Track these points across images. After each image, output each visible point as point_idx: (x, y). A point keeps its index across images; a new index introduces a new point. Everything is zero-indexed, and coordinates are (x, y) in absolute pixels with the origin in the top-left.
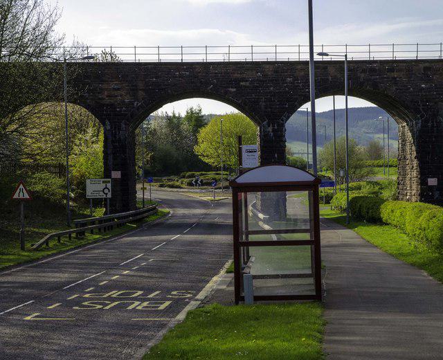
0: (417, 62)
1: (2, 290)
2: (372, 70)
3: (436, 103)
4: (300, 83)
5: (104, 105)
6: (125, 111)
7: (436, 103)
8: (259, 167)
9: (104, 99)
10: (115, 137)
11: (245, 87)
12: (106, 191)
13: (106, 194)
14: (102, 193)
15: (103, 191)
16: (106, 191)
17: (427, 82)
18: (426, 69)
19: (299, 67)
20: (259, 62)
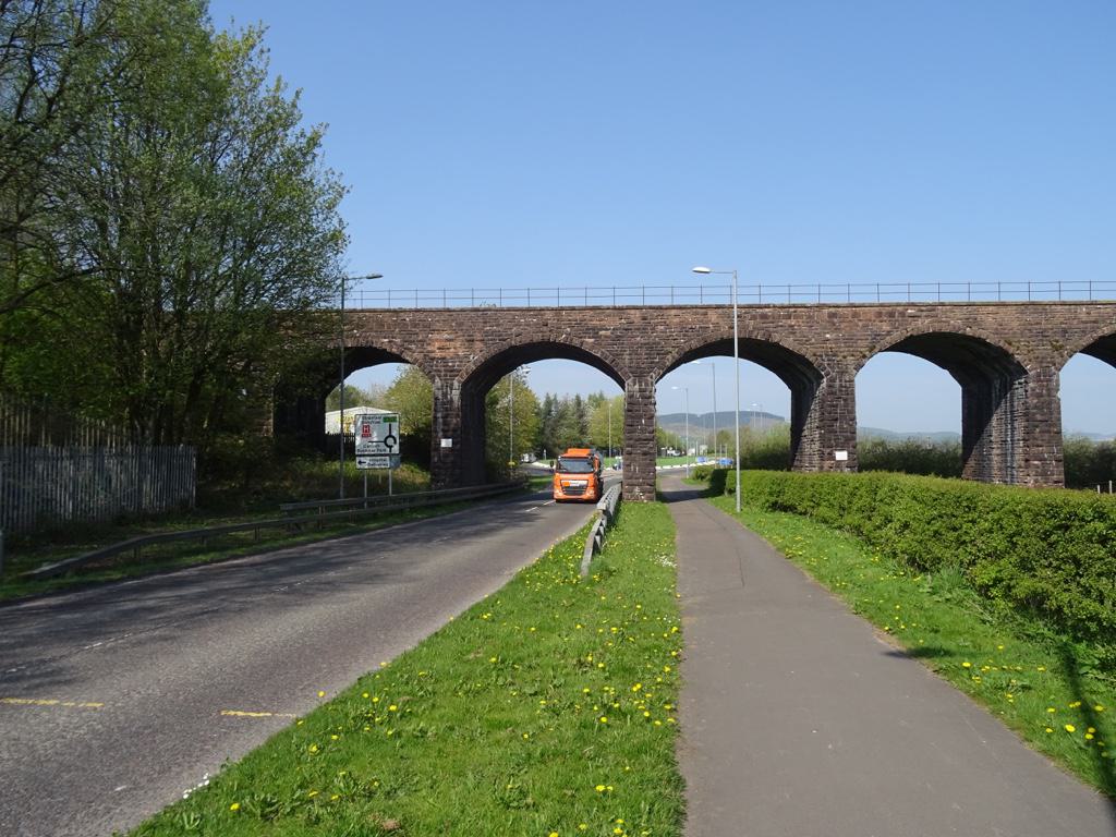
5: (433, 359)
11: (606, 337)
12: (390, 442)
13: (391, 447)
14: (382, 446)
16: (390, 442)
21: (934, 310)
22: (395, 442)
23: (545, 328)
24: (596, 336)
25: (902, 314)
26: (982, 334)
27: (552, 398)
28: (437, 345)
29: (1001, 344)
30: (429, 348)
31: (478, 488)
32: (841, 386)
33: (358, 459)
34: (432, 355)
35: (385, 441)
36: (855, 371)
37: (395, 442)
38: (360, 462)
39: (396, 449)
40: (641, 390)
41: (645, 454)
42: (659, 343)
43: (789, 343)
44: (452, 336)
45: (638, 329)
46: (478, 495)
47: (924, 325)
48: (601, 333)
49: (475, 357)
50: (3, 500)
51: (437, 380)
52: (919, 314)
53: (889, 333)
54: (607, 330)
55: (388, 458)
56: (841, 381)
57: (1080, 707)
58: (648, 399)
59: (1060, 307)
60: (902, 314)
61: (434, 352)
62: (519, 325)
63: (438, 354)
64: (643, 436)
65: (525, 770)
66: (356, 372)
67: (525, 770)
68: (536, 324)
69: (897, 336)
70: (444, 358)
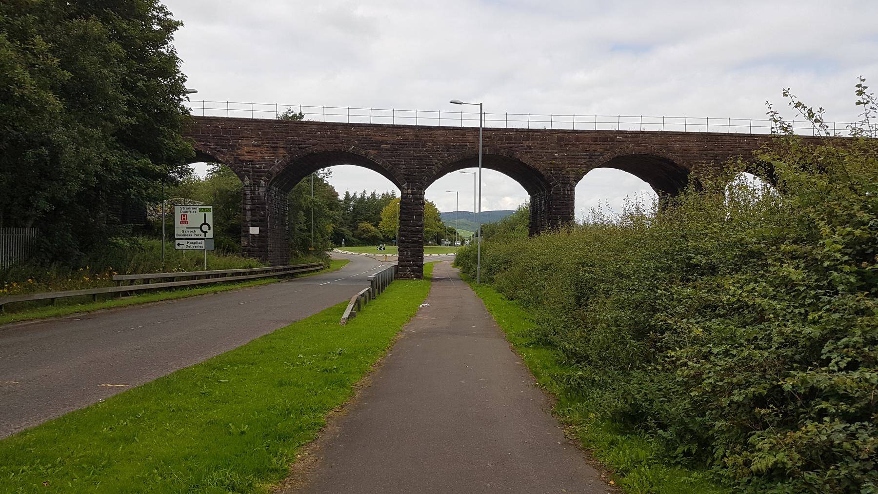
0: (552, 131)
1: (2, 327)
2: (509, 138)
3: (567, 172)
4: (439, 148)
5: (243, 161)
6: (264, 168)
7: (567, 172)
8: (454, 279)
9: (244, 155)
10: (254, 194)
11: (386, 149)
12: (205, 228)
13: (205, 233)
14: (198, 231)
15: (201, 228)
16: (205, 228)
17: (560, 152)
18: (560, 139)
19: (439, 132)
20: (400, 125)
21: (636, 137)
22: (209, 229)
23: (337, 141)
24: (378, 148)
25: (613, 140)
26: (671, 156)
27: (351, 195)
28: (247, 149)
29: (685, 164)
30: (239, 152)
31: (281, 267)
32: (564, 194)
33: (177, 242)
34: (242, 158)
35: (201, 228)
36: (575, 183)
37: (209, 229)
38: (179, 245)
39: (210, 234)
40: (413, 193)
41: (415, 242)
42: (427, 157)
43: (526, 159)
44: (259, 143)
45: (412, 145)
46: (282, 273)
47: (630, 148)
48: (382, 146)
49: (278, 162)
50: (2, 262)
51: (246, 178)
52: (625, 139)
53: (602, 154)
54: (387, 144)
55: (203, 241)
56: (564, 190)
57: (692, 452)
58: (419, 200)
59: (728, 138)
60: (613, 140)
61: (244, 155)
62: (316, 136)
63: (247, 157)
64: (413, 229)
65: (630, 413)
66: (436, 181)
67: (630, 413)
68: (330, 137)
69: (607, 156)
70: (252, 161)
